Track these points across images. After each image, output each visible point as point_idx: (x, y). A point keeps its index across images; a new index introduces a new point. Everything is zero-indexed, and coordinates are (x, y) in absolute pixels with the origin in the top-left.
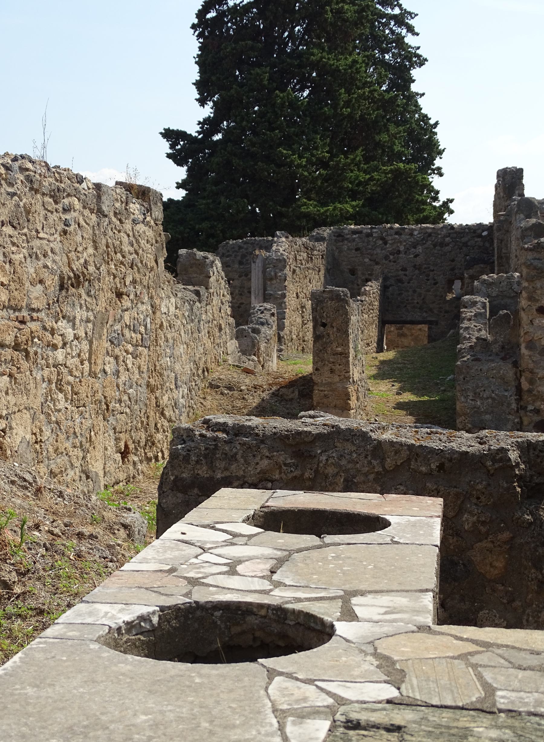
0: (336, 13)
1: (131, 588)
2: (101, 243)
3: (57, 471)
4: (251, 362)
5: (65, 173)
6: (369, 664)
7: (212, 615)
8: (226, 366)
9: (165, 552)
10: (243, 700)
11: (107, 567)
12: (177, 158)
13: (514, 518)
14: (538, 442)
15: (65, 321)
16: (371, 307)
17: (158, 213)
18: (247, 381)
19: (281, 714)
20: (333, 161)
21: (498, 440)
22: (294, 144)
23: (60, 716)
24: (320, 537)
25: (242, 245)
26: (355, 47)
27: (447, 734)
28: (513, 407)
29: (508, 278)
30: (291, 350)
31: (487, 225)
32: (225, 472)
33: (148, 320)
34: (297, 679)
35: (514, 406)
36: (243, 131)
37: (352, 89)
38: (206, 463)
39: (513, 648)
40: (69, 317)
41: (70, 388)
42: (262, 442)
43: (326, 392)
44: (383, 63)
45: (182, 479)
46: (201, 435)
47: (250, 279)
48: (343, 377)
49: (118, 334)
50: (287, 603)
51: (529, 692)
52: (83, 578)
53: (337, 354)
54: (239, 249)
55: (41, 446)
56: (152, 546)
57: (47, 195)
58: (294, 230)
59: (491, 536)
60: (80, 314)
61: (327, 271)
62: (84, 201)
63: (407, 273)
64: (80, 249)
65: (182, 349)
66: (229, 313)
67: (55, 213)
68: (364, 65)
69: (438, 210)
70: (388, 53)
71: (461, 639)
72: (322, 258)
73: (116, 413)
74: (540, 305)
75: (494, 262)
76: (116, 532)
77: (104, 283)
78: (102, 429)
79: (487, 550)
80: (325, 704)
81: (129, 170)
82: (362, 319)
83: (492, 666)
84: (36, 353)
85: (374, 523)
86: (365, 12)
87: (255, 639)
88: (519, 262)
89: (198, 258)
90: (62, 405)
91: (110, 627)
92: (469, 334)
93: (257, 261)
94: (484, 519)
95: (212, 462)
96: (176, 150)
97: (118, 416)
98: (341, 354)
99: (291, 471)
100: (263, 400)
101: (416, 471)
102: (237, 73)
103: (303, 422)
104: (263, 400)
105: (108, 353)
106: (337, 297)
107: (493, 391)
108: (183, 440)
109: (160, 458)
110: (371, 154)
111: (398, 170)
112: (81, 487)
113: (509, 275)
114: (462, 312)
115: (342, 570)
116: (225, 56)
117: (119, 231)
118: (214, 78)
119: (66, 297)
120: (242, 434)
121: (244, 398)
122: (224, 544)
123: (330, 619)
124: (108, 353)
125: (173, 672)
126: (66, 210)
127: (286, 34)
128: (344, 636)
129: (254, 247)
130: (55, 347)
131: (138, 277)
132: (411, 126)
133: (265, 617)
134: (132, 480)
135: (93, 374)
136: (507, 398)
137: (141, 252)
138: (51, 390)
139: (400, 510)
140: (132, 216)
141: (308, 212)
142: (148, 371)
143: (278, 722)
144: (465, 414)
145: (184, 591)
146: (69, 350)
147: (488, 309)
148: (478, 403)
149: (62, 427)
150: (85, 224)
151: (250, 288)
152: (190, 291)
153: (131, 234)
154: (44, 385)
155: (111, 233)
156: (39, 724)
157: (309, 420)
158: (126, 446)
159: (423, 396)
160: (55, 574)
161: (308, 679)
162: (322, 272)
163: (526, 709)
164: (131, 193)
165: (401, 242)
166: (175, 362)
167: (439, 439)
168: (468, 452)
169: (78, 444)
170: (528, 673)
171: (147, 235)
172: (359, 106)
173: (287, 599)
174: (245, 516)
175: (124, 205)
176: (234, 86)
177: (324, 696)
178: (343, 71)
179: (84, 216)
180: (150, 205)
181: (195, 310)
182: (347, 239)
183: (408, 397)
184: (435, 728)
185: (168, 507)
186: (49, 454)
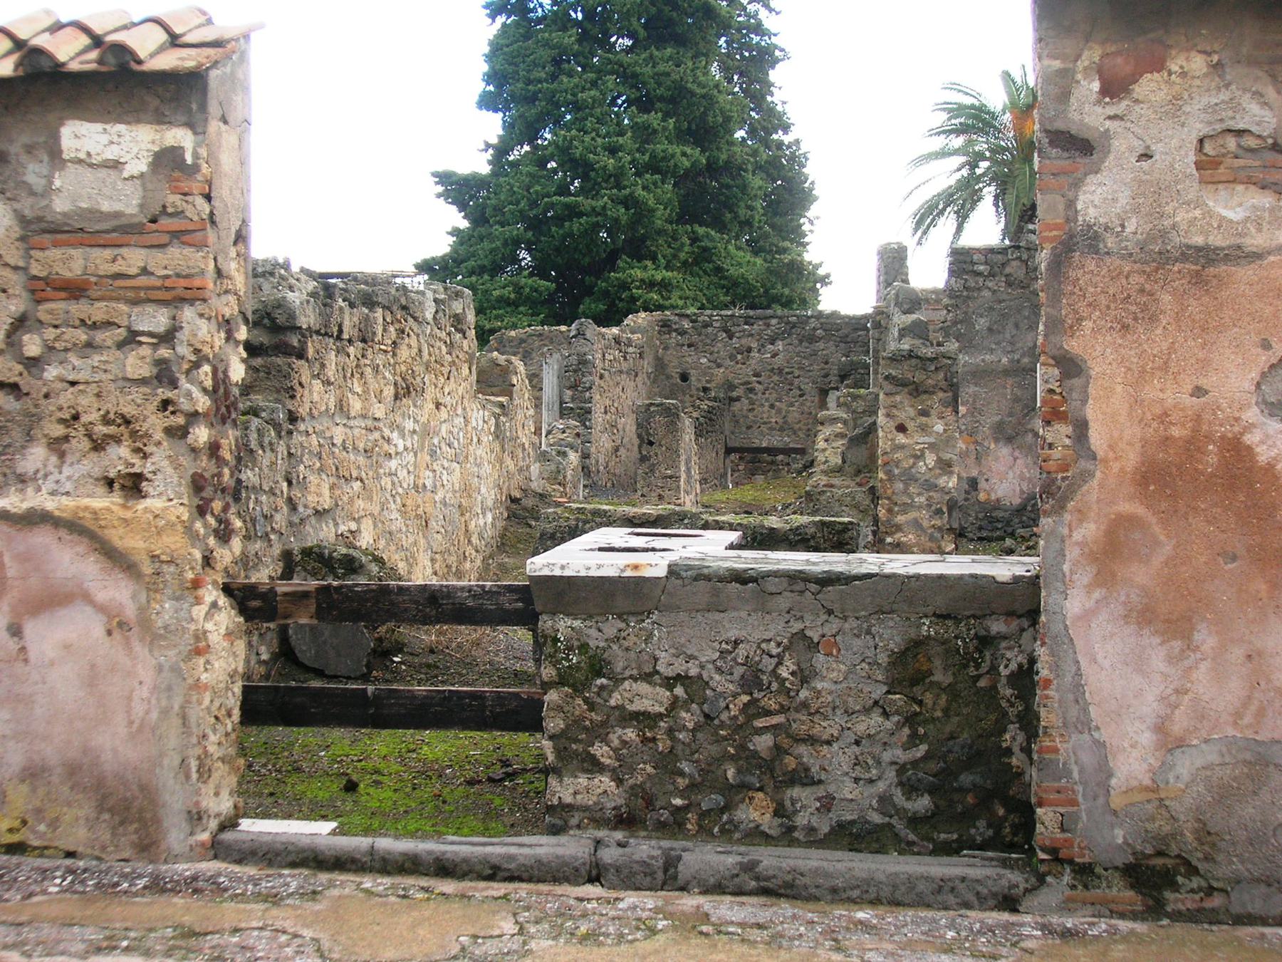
60: (409, 425)
98: (671, 477)
116: (526, 77)
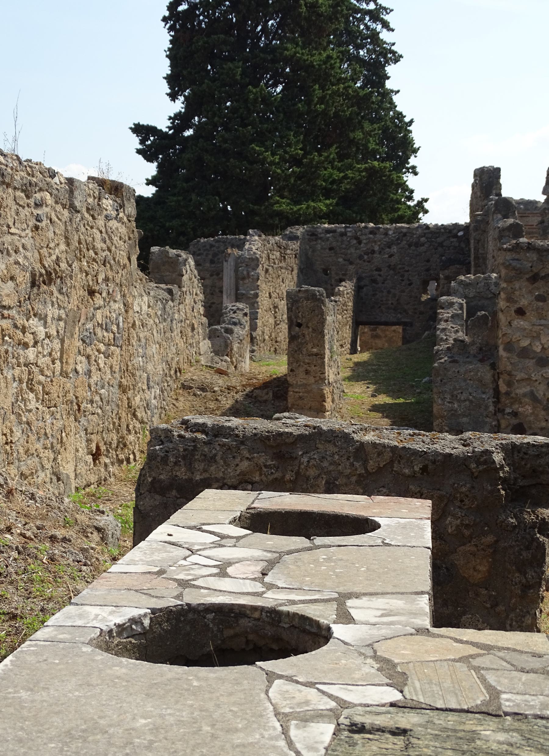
0: (310, 7)
1: (120, 590)
2: (73, 239)
3: (28, 472)
4: (223, 363)
5: (37, 167)
6: (370, 668)
7: (205, 618)
8: (198, 367)
9: (153, 553)
10: (244, 704)
11: (81, 571)
12: (147, 154)
13: (498, 522)
14: (522, 444)
15: (36, 319)
16: (345, 308)
17: (131, 209)
18: (220, 382)
19: (284, 718)
20: (306, 158)
21: (482, 442)
22: (266, 141)
23: (56, 720)
24: (310, 539)
25: (214, 243)
26: (330, 42)
27: (454, 738)
28: (491, 409)
29: (485, 279)
30: (263, 351)
31: (462, 225)
32: (204, 474)
33: (121, 319)
34: (297, 682)
35: (492, 408)
36: (216, 126)
37: (326, 85)
38: (185, 464)
39: (515, 650)
40: (41, 315)
41: (41, 388)
42: (242, 443)
43: (301, 394)
44: (358, 58)
45: (160, 481)
46: (180, 436)
47: (222, 279)
48: (318, 378)
49: (90, 333)
50: (281, 605)
51: (533, 695)
52: (56, 582)
53: (312, 355)
54: (211, 248)
55: (11, 447)
56: (139, 548)
57: (18, 189)
58: (267, 229)
59: (475, 540)
60: (52, 312)
61: (301, 270)
62: (56, 196)
63: (382, 273)
64: (52, 245)
65: (154, 348)
66: (202, 313)
67: (26, 208)
68: (338, 61)
69: (413, 209)
70: (362, 49)
71: (461, 642)
72: (296, 257)
73: (87, 413)
74: (518, 306)
75: (470, 263)
76: (89, 535)
77: (76, 281)
78: (73, 430)
79: (471, 554)
80: (328, 707)
81: (101, 164)
82: (337, 318)
83: (494, 669)
84: (7, 352)
85: (363, 525)
86: (340, 6)
87: (248, 642)
88: (496, 263)
89: (170, 256)
90: (32, 405)
91: (101, 630)
92: (446, 335)
93: (230, 260)
94: (467, 522)
95: (190, 464)
96: (146, 145)
97: (90, 417)
98: (316, 355)
99: (272, 473)
100: (237, 401)
101: (398, 474)
102: (209, 67)
103: (283, 423)
104: (237, 401)
105: (79, 352)
106: (312, 297)
107: (470, 394)
108: (161, 441)
109: (132, 460)
110: (346, 151)
111: (373, 168)
112: (52, 489)
113: (486, 275)
114: (439, 313)
115: (334, 572)
117: (92, 228)
118: (185, 72)
119: (38, 294)
120: (221, 435)
121: (217, 400)
122: (212, 545)
123: (326, 622)
124: (79, 352)
125: (170, 675)
126: (38, 205)
127: (259, 28)
128: (342, 639)
129: (225, 245)
130: (26, 346)
131: (110, 274)
132: (385, 124)
133: (258, 619)
134: (103, 482)
135: (64, 374)
136: (484, 401)
137: (113, 249)
138: (22, 390)
139: (389, 512)
140: (105, 212)
141: (281, 210)
142: (120, 371)
143: (281, 725)
144: (442, 417)
145: (175, 594)
146: (40, 349)
147: (465, 310)
148: (456, 406)
149: (33, 428)
150: (57, 220)
151: (222, 287)
152: (163, 289)
153: (104, 230)
154: (15, 385)
155: (83, 229)
156: (36, 728)
157: (288, 421)
158: (98, 448)
159: (399, 398)
160: (28, 578)
161: (308, 682)
162: (296, 271)
163: (532, 712)
164: (103, 189)
165: (375, 242)
166: (147, 362)
167: (420, 442)
168: (451, 454)
169: (49, 446)
170: (532, 676)
171: (120, 232)
172: (333, 102)
173: (280, 602)
174: (231, 518)
175: (96, 200)
176: (206, 81)
177: (326, 699)
178: (317, 67)
179: (56, 211)
180: (123, 201)
181: (168, 309)
182: (321, 238)
183: (383, 399)
184: (441, 731)
185: (145, 509)
186: (19, 456)
